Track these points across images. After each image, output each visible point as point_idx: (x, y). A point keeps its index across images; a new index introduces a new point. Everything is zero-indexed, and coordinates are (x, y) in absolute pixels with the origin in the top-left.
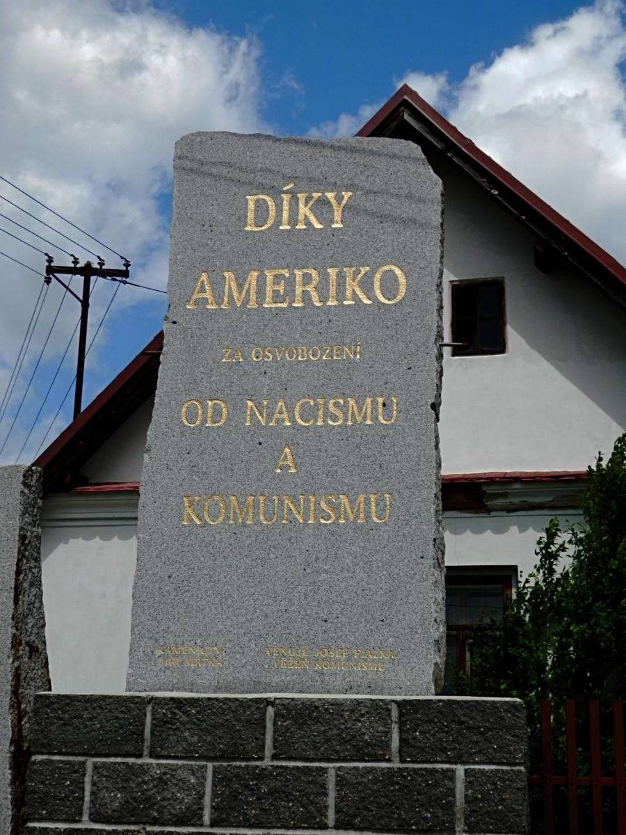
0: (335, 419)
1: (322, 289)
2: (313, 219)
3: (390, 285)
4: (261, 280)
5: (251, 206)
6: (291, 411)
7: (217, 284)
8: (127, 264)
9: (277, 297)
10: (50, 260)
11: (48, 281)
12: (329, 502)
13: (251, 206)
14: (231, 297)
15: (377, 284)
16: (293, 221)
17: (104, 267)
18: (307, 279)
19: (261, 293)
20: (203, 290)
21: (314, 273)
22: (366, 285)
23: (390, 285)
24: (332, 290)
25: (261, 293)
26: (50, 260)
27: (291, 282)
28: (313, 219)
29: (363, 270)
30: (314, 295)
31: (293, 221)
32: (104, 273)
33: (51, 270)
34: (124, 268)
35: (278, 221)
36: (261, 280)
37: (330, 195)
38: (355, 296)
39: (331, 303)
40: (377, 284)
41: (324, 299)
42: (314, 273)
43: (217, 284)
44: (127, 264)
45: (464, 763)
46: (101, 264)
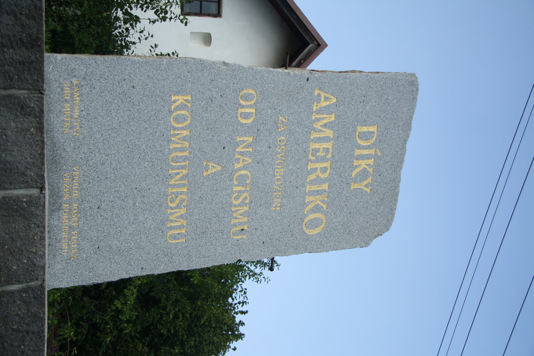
3: (314, 224)
4: (326, 139)
6: (244, 168)
7: (328, 110)
9: (317, 150)
14: (319, 120)
18: (324, 170)
19: (319, 140)
20: (326, 99)
21: (326, 175)
22: (317, 209)
23: (314, 224)
24: (314, 188)
27: (323, 159)
29: (325, 207)
30: (312, 177)
36: (326, 139)
41: (311, 183)
43: (328, 110)
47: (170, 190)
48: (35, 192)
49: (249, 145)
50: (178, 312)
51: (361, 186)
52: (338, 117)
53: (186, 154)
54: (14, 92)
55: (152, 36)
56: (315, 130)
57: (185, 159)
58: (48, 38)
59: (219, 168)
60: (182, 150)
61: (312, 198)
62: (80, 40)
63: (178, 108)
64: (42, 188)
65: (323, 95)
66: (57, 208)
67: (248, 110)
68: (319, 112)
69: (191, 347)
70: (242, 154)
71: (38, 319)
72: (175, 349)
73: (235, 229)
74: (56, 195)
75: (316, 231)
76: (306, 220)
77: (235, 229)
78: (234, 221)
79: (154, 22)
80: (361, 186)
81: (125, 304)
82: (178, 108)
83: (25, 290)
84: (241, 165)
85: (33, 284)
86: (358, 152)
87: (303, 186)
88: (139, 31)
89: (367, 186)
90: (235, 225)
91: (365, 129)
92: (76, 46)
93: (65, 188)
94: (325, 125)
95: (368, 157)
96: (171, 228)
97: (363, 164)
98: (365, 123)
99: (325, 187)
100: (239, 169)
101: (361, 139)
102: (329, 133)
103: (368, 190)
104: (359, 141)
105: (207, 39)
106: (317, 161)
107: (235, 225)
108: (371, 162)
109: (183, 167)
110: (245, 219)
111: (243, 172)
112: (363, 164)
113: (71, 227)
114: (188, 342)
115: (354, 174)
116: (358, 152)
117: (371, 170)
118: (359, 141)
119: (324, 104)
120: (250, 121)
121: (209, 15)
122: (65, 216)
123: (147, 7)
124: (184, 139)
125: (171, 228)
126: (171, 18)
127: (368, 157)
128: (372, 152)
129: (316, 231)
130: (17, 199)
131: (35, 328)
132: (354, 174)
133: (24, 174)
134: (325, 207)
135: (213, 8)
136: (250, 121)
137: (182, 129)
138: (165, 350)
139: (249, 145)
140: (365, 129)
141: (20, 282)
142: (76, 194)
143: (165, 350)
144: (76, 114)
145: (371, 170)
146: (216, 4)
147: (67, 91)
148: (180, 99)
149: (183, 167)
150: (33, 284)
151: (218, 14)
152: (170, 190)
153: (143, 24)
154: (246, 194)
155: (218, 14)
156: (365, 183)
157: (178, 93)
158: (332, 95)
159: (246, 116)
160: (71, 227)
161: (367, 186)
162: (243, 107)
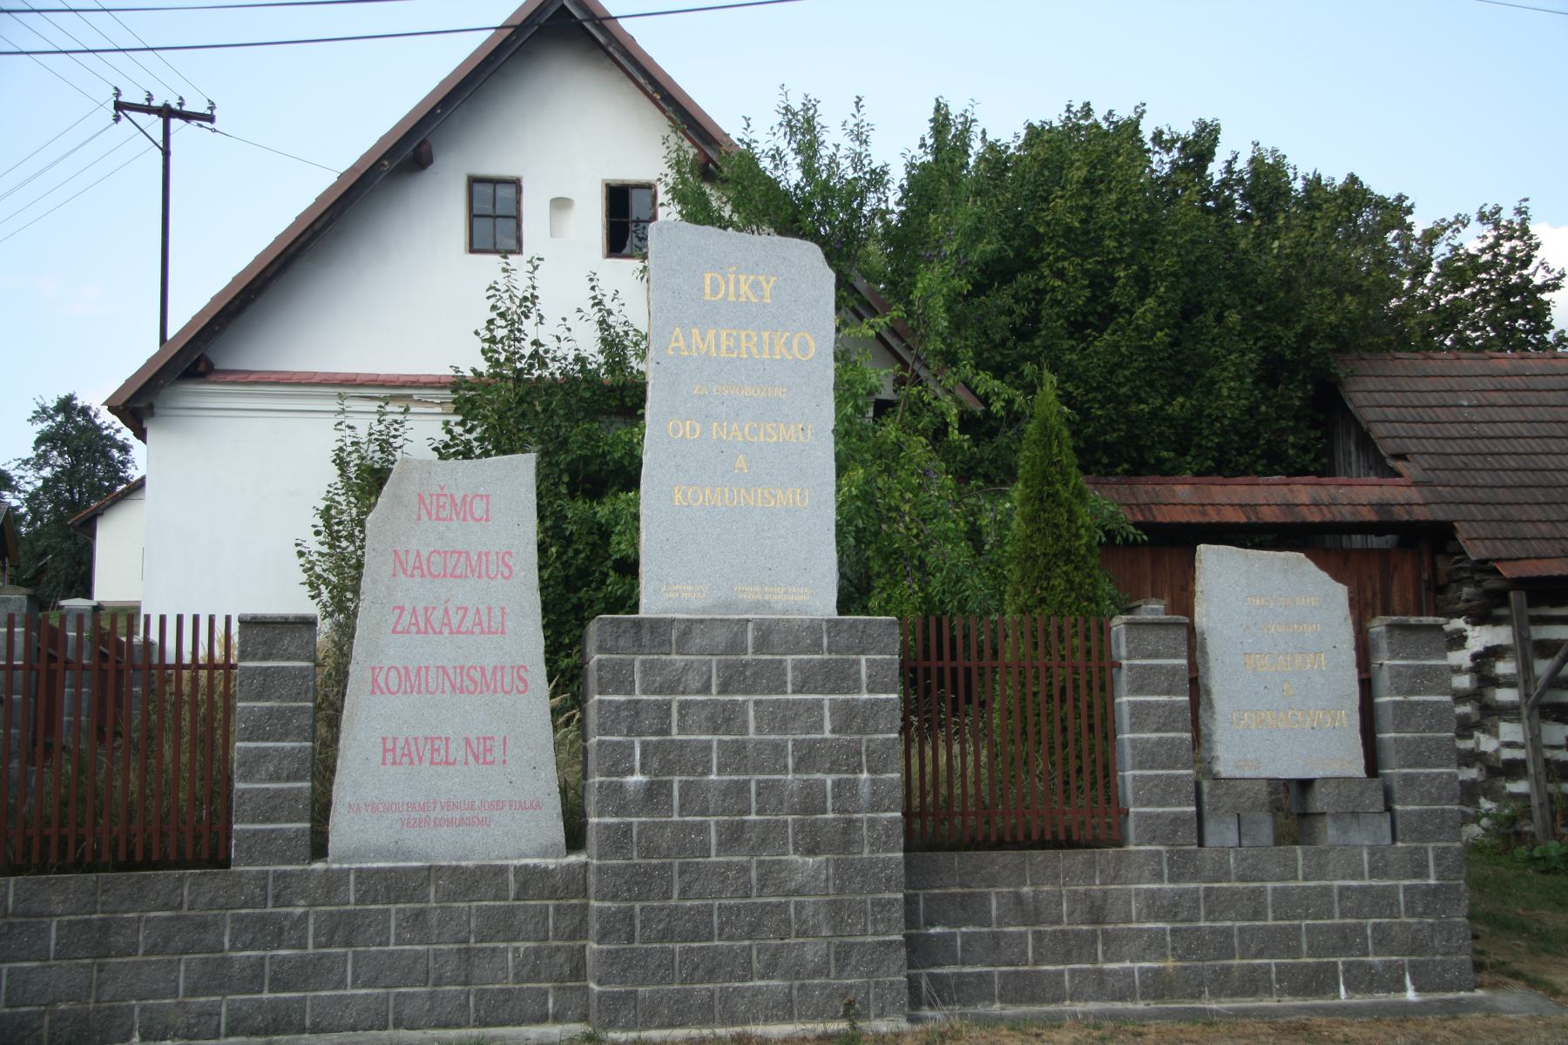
0: (771, 437)
1: (759, 344)
2: (750, 295)
3: (804, 348)
4: (717, 336)
5: (708, 281)
6: (742, 430)
7: (687, 336)
8: (212, 107)
9: (729, 350)
10: (118, 93)
11: (117, 119)
12: (770, 492)
13: (708, 281)
14: (697, 347)
15: (795, 345)
16: (738, 295)
17: (184, 108)
18: (748, 337)
19: (718, 346)
20: (677, 340)
21: (753, 334)
22: (788, 345)
23: (804, 348)
24: (766, 347)
25: (718, 346)
26: (118, 93)
27: (737, 339)
28: (750, 295)
29: (787, 334)
30: (754, 351)
31: (738, 295)
32: (188, 117)
33: (120, 106)
34: (209, 112)
35: (726, 295)
36: (717, 336)
37: (762, 278)
38: (781, 353)
39: (766, 356)
40: (795, 345)
41: (760, 352)
42: (753, 334)
43: (687, 336)
44: (212, 108)
45: (639, 735)
46: (181, 105)
47: (760, 505)
48: (750, 626)
49: (720, 425)
50: (1051, 270)
51: (767, 288)
52: (695, 324)
53: (726, 490)
54: (673, 639)
55: (564, 319)
56: (707, 352)
57: (730, 490)
58: (829, 1031)
59: (741, 457)
60: (723, 494)
61: (777, 350)
62: (579, 448)
63: (685, 499)
64: (748, 620)
65: (674, 344)
66: (767, 606)
67: (688, 428)
68: (689, 348)
69: (1120, 246)
70: (728, 434)
71: (854, 624)
72: (1119, 277)
73: (802, 439)
74: (757, 606)
75: (812, 344)
76: (799, 356)
77: (802, 439)
78: (793, 440)
79: (541, 317)
80: (767, 288)
81: (998, 394)
82: (685, 499)
83: (829, 634)
84: (739, 434)
85: (824, 628)
86: (732, 298)
87: (763, 363)
88: (557, 344)
89: (768, 282)
90: (797, 438)
91: (708, 290)
92: (589, 453)
93: (752, 597)
94: (703, 339)
95: (737, 281)
96: (794, 503)
97: (744, 288)
98: (702, 290)
99: (766, 335)
100: (743, 435)
101: (717, 294)
102: (711, 334)
103: (773, 279)
104: (720, 296)
105: (560, 204)
106: (738, 346)
107: (797, 438)
108: (742, 278)
109: (739, 493)
110: (792, 427)
111: (746, 430)
112: (744, 288)
113: (785, 593)
114: (1109, 253)
115: (755, 300)
116: (732, 298)
117: (752, 277)
118: (720, 296)
119: (682, 344)
120: (698, 427)
121: (519, 202)
122: (775, 597)
123: (520, 330)
124: (713, 492)
125: (794, 503)
126: (534, 288)
127: (737, 281)
128: (732, 277)
129: (812, 344)
130: (756, 639)
131: (861, 627)
132: (755, 300)
133: (736, 634)
134: (787, 334)
135: (505, 192)
136: (698, 427)
137: (704, 494)
138: (1117, 295)
139: (720, 425)
140: (708, 290)
141: (821, 638)
142: (757, 589)
143: (1117, 295)
144: (690, 588)
145: (752, 277)
146: (499, 187)
147: (671, 595)
148: (678, 496)
149: (739, 493)
150: (824, 628)
151: (516, 184)
152: (760, 505)
153: (546, 335)
154: (768, 427)
155: (516, 184)
156: (764, 284)
157: (673, 500)
158: (672, 333)
159: (693, 430)
160: (785, 593)
161: (768, 282)
162: (684, 434)
